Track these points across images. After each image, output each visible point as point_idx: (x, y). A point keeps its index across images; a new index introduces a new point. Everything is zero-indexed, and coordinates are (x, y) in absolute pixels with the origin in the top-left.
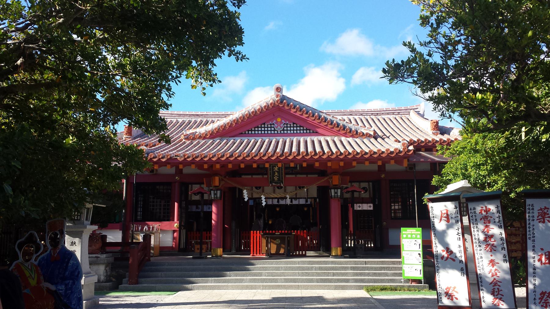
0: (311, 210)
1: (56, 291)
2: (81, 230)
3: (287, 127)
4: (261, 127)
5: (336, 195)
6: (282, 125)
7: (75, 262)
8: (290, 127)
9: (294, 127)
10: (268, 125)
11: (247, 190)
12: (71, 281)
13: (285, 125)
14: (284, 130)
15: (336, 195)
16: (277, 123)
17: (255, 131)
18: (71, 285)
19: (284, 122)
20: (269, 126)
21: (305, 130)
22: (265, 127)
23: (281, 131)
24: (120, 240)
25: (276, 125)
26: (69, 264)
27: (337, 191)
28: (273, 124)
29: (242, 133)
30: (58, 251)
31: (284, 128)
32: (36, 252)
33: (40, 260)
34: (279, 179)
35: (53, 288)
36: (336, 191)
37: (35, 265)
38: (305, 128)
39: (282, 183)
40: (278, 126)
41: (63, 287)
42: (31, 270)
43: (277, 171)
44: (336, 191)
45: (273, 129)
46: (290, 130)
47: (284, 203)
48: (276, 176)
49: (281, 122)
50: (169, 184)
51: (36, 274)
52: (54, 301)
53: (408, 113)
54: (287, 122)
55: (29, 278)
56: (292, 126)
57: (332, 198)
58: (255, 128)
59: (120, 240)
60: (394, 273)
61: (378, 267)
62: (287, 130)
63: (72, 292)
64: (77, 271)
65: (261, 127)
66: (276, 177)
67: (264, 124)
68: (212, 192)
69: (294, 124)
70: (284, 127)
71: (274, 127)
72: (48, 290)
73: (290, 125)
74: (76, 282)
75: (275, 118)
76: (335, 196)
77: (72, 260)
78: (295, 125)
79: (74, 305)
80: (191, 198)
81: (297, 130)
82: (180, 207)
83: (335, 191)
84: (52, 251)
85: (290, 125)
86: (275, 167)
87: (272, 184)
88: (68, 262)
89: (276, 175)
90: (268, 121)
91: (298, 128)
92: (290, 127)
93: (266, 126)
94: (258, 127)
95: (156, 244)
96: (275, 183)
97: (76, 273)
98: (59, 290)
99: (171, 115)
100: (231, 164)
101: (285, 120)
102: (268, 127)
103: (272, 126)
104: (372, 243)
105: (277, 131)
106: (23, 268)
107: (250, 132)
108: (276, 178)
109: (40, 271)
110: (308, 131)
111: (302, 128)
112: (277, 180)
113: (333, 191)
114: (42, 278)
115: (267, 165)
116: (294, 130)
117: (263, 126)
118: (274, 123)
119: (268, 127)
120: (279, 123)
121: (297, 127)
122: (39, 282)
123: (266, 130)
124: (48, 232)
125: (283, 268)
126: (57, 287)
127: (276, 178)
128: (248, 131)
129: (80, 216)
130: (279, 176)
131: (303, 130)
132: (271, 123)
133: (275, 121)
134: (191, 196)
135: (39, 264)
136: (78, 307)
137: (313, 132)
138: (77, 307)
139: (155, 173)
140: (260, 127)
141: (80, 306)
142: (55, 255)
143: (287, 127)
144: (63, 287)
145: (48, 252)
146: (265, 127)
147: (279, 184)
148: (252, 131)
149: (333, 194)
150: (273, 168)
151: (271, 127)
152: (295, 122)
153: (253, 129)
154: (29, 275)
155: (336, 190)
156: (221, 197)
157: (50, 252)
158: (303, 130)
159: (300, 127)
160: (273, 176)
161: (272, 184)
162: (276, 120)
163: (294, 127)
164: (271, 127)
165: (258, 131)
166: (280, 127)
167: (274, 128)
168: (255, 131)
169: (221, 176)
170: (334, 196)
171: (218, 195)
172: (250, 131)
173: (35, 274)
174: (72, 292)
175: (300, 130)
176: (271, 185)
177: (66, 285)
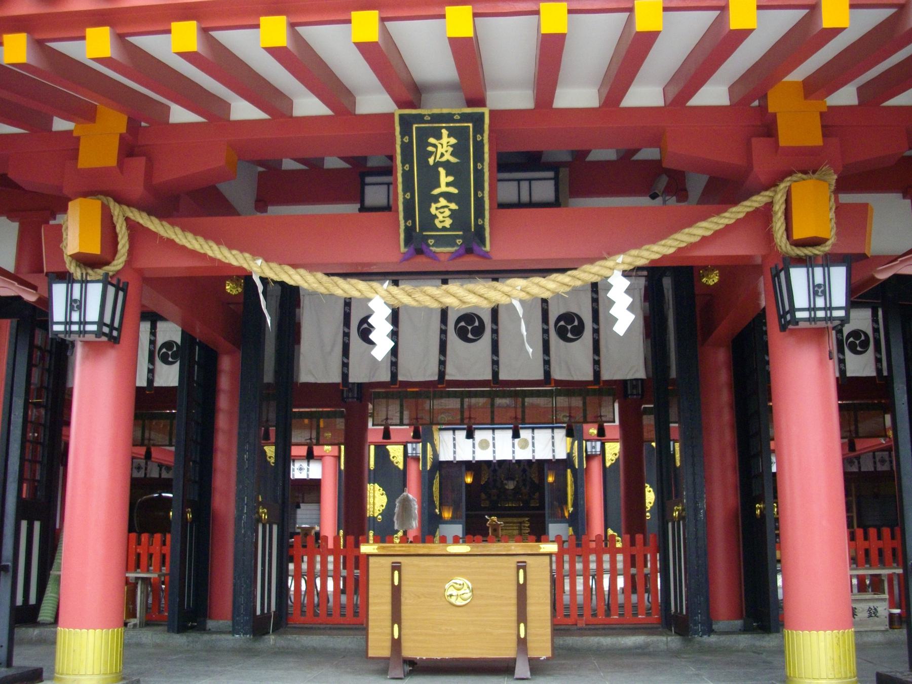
5: (820, 302)
15: (820, 302)
24: (305, 377)
27: (827, 277)
43: (447, 165)
44: (819, 279)
47: (529, 457)
48: (446, 195)
59: (305, 377)
66: (443, 202)
76: (812, 309)
82: (195, 358)
83: (810, 278)
86: (439, 137)
89: (443, 188)
104: (673, 412)
125: (480, 222)
130: (460, 199)
149: (801, 299)
155: (818, 271)
160: (428, 199)
170: (808, 309)
171: (93, 314)
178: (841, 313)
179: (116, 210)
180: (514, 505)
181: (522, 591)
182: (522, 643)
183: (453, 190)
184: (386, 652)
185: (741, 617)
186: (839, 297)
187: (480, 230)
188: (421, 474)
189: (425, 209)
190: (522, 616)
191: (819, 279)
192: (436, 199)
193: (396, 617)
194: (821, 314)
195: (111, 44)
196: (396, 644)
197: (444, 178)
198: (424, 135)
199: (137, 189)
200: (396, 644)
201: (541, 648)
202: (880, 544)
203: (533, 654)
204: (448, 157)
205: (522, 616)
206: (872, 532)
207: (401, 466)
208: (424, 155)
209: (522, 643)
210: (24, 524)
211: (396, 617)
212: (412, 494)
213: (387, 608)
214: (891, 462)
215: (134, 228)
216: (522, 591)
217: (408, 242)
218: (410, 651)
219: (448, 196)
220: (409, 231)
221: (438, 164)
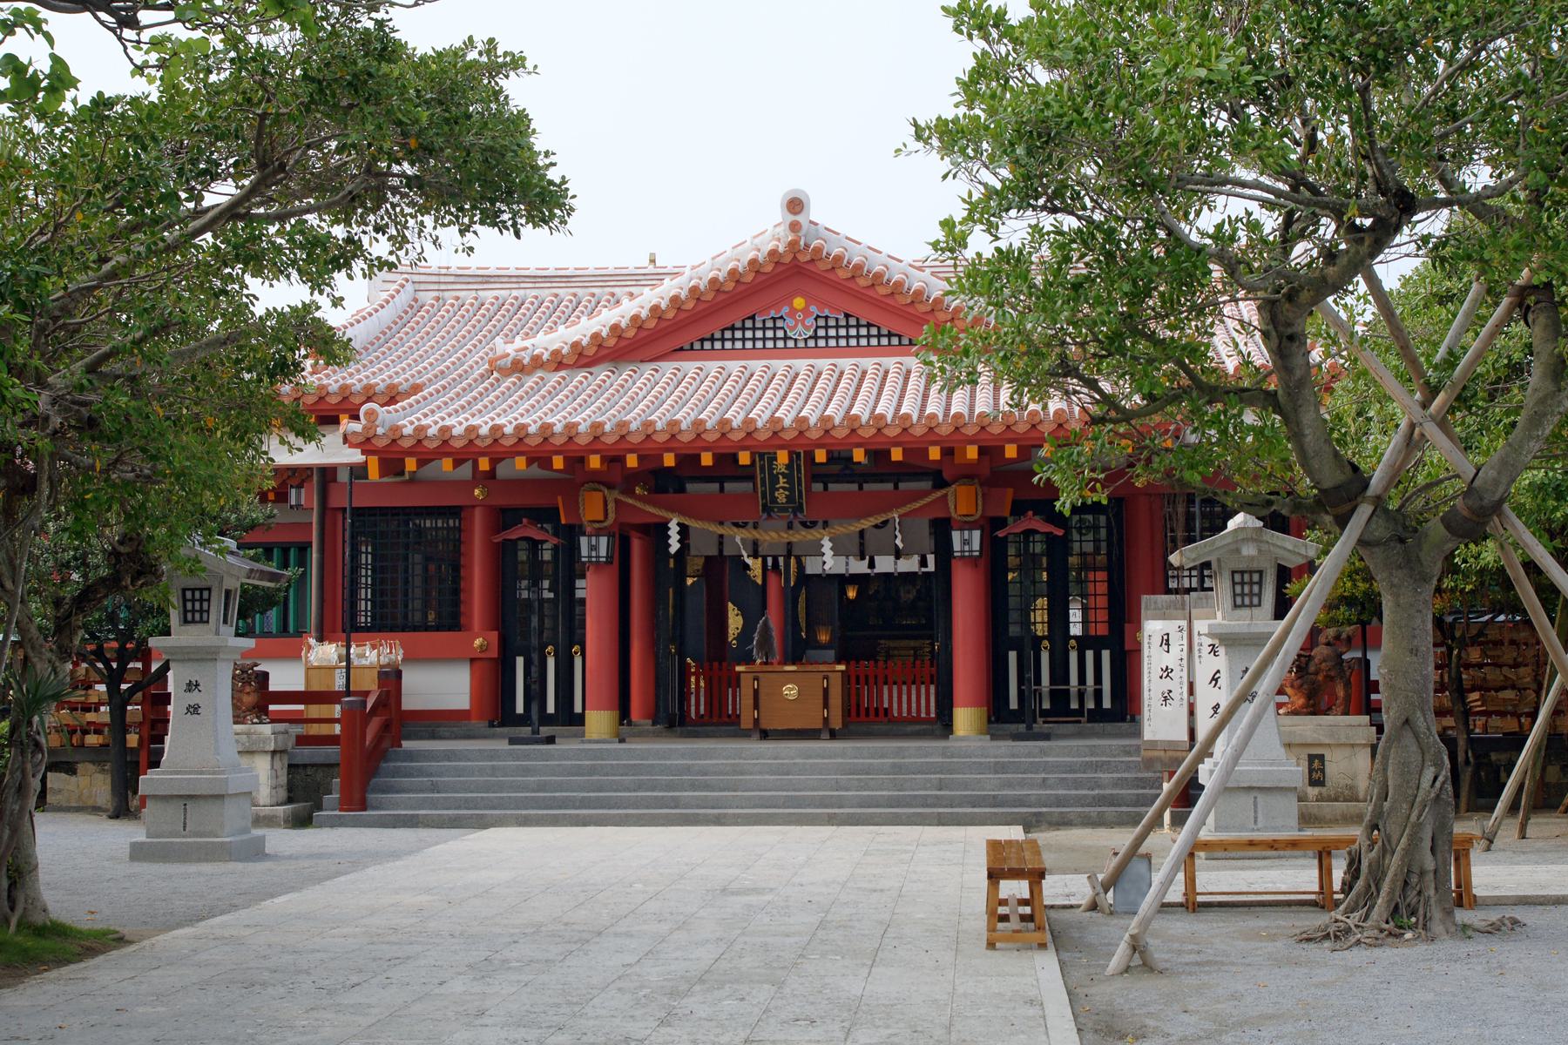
3: (827, 327)
4: (743, 329)
5: (594, 554)
6: (810, 321)
8: (837, 327)
9: (847, 327)
13: (821, 322)
16: (793, 312)
17: (723, 340)
19: (817, 312)
22: (754, 329)
23: (806, 340)
29: (681, 349)
31: (816, 331)
34: (790, 499)
40: (796, 326)
43: (783, 474)
44: (966, 537)
48: (784, 488)
50: (454, 512)
58: (723, 331)
65: (743, 329)
67: (753, 318)
69: (847, 316)
75: (788, 299)
85: (837, 320)
92: (837, 327)
101: (822, 304)
102: (764, 329)
103: (779, 323)
105: (796, 340)
107: (707, 345)
108: (781, 496)
117: (728, 334)
118: (782, 313)
119: (764, 329)
121: (858, 326)
127: (781, 496)
130: (791, 490)
132: (773, 313)
143: (827, 327)
146: (754, 329)
148: (712, 339)
151: (775, 329)
155: (966, 533)
158: (879, 336)
160: (774, 489)
162: (791, 305)
163: (847, 327)
164: (775, 329)
165: (733, 340)
168: (723, 340)
171: (603, 552)
181: (826, 691)
182: (826, 720)
184: (751, 726)
185: (497, 629)
187: (801, 504)
188: (783, 591)
189: (772, 494)
190: (826, 705)
191: (966, 537)
192: (778, 489)
193: (756, 706)
196: (756, 721)
197: (782, 480)
200: (756, 721)
201: (836, 723)
203: (832, 726)
205: (826, 705)
207: (759, 581)
208: (771, 469)
209: (826, 720)
210: (1090, 654)
211: (756, 706)
212: (773, 617)
213: (751, 702)
215: (617, 501)
216: (826, 691)
217: (764, 511)
218: (764, 725)
219: (784, 488)
220: (764, 506)
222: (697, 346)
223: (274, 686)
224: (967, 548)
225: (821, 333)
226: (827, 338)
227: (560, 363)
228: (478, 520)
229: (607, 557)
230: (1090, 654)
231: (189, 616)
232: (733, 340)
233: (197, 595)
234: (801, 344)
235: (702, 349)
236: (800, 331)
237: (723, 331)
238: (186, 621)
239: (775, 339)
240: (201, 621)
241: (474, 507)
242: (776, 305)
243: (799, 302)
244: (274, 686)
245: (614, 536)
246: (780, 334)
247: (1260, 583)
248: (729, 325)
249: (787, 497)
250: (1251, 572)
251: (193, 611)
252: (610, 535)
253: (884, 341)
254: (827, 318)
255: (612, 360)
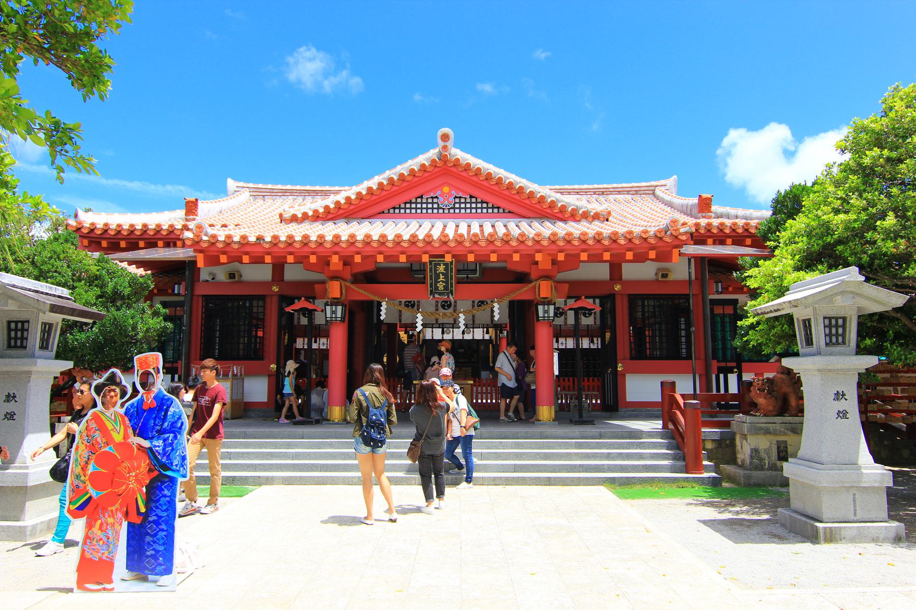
0: (491, 348)
1: (150, 449)
2: (26, 368)
3: (460, 203)
4: (416, 203)
5: (334, 316)
6: (451, 199)
7: (177, 410)
8: (465, 203)
9: (471, 203)
10: (427, 199)
11: (387, 303)
12: (171, 435)
13: (457, 200)
14: (454, 208)
15: (546, 315)
16: (442, 194)
17: (405, 208)
18: (171, 440)
19: (455, 194)
20: (430, 200)
21: (490, 208)
22: (422, 203)
23: (449, 209)
25: (441, 199)
26: (169, 413)
28: (437, 197)
29: (383, 212)
30: (153, 395)
31: (454, 204)
32: (122, 397)
33: (127, 407)
34: (446, 288)
35: (146, 444)
36: (334, 310)
37: (121, 415)
38: (490, 205)
39: (452, 295)
40: (444, 201)
41: (160, 443)
42: (115, 420)
43: (442, 273)
44: (546, 309)
45: (435, 206)
46: (466, 208)
48: (441, 281)
49: (450, 194)
50: (262, 298)
51: (122, 427)
52: (148, 461)
53: (651, 192)
54: (460, 195)
55: (112, 432)
56: (468, 200)
57: (538, 320)
58: (416, 198)
60: (654, 454)
61: (625, 442)
62: (460, 208)
63: (172, 450)
64: (180, 421)
65: (416, 203)
66: (441, 283)
67: (421, 197)
68: (328, 308)
69: (471, 197)
70: (455, 203)
71: (437, 203)
72: (140, 447)
73: (465, 198)
74: (179, 436)
75: (440, 186)
77: (173, 407)
78: (474, 200)
79: (176, 465)
80: (299, 322)
81: (476, 208)
83: (544, 308)
84: (145, 396)
85: (465, 198)
87: (434, 297)
88: (167, 411)
89: (441, 279)
90: (430, 191)
91: (479, 205)
92: (465, 203)
93: (424, 201)
94: (411, 203)
95: (235, 397)
96: (439, 295)
97: (179, 424)
98: (155, 446)
99: (271, 190)
100: (359, 256)
101: (458, 189)
102: (427, 203)
103: (435, 200)
105: (444, 209)
106: (103, 418)
107: (397, 211)
108: (441, 286)
109: (128, 422)
110: (496, 211)
111: (485, 205)
112: (442, 289)
113: (540, 308)
114: (130, 431)
115: (425, 258)
116: (471, 208)
117: (419, 200)
119: (427, 203)
120: (446, 193)
121: (476, 203)
122: (126, 437)
123: (425, 208)
124: (138, 370)
126: (152, 442)
127: (441, 286)
128: (394, 208)
129: (9, 338)
130: (446, 282)
131: (487, 208)
132: (432, 195)
133: (439, 192)
134: (299, 318)
135: (126, 413)
136: (181, 469)
137: (504, 212)
138: (180, 468)
139: (236, 279)
140: (413, 203)
141: (185, 467)
142: (149, 402)
143: (460, 203)
144: (160, 443)
145: (139, 397)
146: (422, 203)
147: (446, 297)
148: (400, 208)
149: (541, 314)
150: (435, 267)
151: (433, 203)
152: (473, 194)
153: (403, 206)
154: (113, 427)
155: (546, 306)
156: (343, 318)
157: (142, 396)
158: (487, 208)
159: (482, 202)
161: (434, 297)
162: (442, 191)
163: (471, 203)
164: (433, 203)
165: (411, 208)
166: (448, 201)
167: (438, 205)
168: (405, 208)
169: (345, 280)
171: (339, 315)
172: (397, 208)
173: (120, 426)
174: (172, 450)
175: (482, 208)
176: (432, 297)
177: (165, 440)
178: (552, 318)
179: (343, 283)
180: (217, 347)
183: (444, 280)
186: (552, 314)
191: (546, 309)
192: (439, 282)
194: (546, 318)
195: (729, 537)
197: (441, 277)
198: (436, 265)
199: (349, 277)
202: (588, 384)
204: (442, 271)
206: (591, 379)
208: (436, 271)
210: (722, 376)
214: (598, 344)
220: (431, 291)
221: (439, 273)
222: (392, 211)
223: (730, 376)
224: (546, 315)
225: (457, 206)
226: (460, 208)
227: (318, 217)
228: (275, 301)
229: (341, 318)
230: (722, 376)
231: (840, 322)
232: (411, 208)
233: (20, 325)
234: (446, 211)
235: (394, 213)
236: (450, 201)
237: (416, 198)
238: (844, 319)
239: (433, 208)
240: (830, 319)
241: (272, 296)
242: (434, 189)
243: (446, 189)
244: (730, 376)
245: (346, 306)
246: (435, 206)
247: (844, 326)
248: (420, 195)
249: (444, 286)
250: (837, 319)
251: (16, 338)
252: (343, 305)
253: (490, 211)
254: (460, 197)
255: (345, 218)
